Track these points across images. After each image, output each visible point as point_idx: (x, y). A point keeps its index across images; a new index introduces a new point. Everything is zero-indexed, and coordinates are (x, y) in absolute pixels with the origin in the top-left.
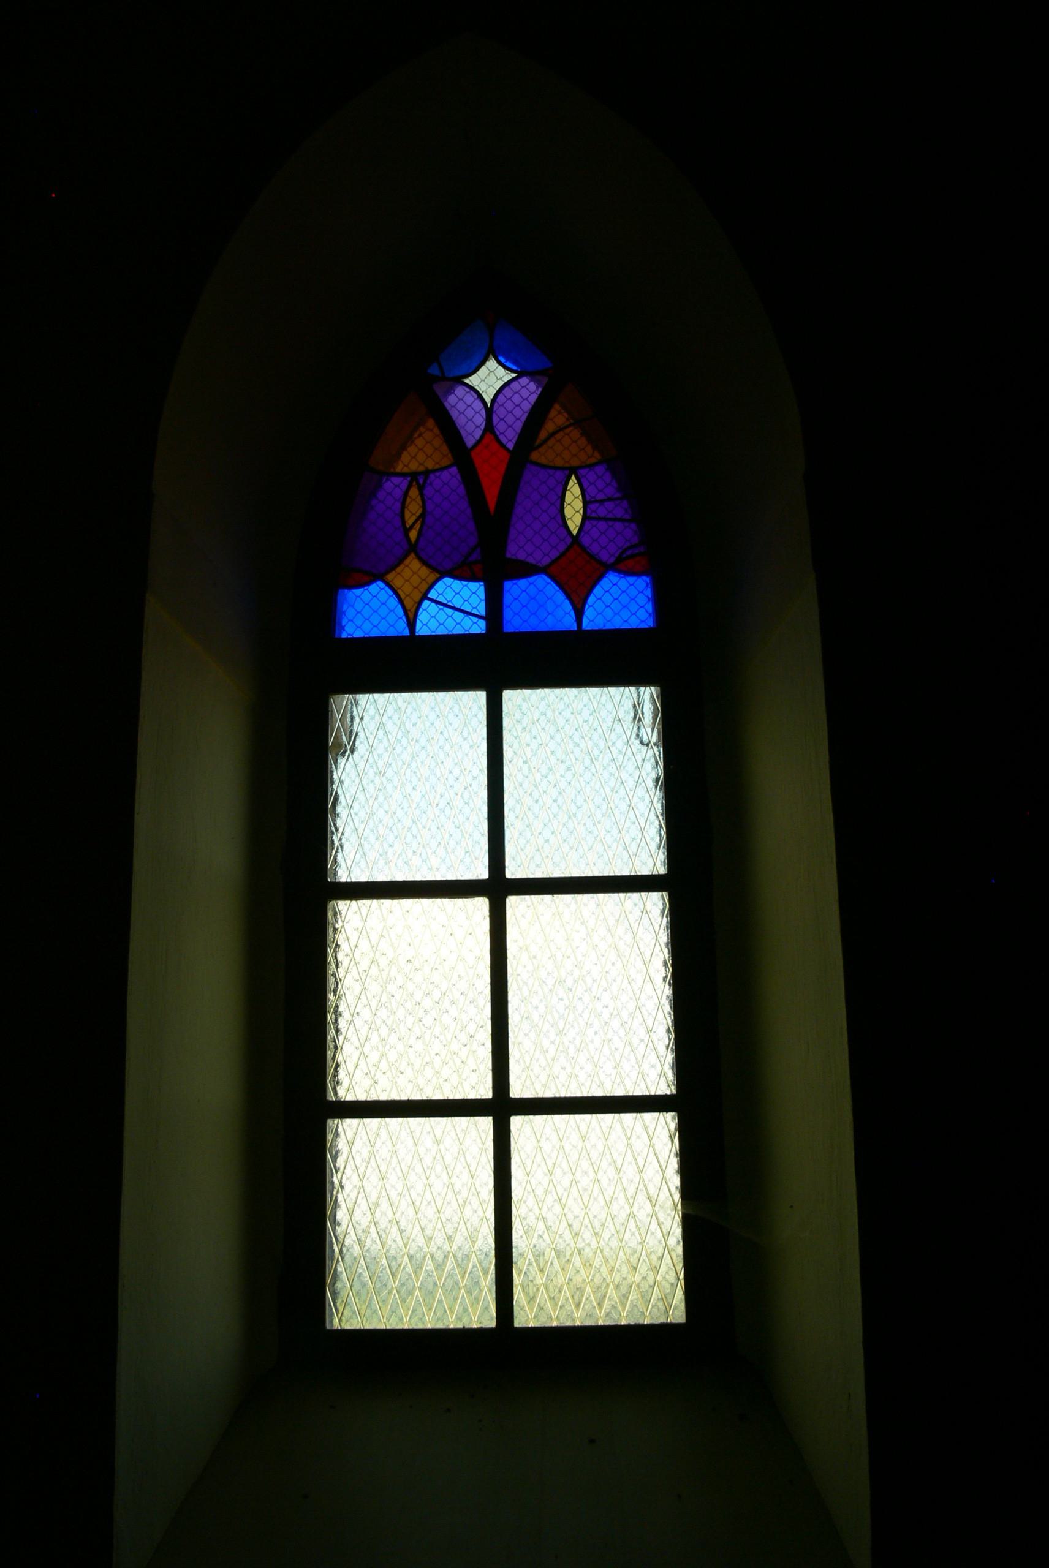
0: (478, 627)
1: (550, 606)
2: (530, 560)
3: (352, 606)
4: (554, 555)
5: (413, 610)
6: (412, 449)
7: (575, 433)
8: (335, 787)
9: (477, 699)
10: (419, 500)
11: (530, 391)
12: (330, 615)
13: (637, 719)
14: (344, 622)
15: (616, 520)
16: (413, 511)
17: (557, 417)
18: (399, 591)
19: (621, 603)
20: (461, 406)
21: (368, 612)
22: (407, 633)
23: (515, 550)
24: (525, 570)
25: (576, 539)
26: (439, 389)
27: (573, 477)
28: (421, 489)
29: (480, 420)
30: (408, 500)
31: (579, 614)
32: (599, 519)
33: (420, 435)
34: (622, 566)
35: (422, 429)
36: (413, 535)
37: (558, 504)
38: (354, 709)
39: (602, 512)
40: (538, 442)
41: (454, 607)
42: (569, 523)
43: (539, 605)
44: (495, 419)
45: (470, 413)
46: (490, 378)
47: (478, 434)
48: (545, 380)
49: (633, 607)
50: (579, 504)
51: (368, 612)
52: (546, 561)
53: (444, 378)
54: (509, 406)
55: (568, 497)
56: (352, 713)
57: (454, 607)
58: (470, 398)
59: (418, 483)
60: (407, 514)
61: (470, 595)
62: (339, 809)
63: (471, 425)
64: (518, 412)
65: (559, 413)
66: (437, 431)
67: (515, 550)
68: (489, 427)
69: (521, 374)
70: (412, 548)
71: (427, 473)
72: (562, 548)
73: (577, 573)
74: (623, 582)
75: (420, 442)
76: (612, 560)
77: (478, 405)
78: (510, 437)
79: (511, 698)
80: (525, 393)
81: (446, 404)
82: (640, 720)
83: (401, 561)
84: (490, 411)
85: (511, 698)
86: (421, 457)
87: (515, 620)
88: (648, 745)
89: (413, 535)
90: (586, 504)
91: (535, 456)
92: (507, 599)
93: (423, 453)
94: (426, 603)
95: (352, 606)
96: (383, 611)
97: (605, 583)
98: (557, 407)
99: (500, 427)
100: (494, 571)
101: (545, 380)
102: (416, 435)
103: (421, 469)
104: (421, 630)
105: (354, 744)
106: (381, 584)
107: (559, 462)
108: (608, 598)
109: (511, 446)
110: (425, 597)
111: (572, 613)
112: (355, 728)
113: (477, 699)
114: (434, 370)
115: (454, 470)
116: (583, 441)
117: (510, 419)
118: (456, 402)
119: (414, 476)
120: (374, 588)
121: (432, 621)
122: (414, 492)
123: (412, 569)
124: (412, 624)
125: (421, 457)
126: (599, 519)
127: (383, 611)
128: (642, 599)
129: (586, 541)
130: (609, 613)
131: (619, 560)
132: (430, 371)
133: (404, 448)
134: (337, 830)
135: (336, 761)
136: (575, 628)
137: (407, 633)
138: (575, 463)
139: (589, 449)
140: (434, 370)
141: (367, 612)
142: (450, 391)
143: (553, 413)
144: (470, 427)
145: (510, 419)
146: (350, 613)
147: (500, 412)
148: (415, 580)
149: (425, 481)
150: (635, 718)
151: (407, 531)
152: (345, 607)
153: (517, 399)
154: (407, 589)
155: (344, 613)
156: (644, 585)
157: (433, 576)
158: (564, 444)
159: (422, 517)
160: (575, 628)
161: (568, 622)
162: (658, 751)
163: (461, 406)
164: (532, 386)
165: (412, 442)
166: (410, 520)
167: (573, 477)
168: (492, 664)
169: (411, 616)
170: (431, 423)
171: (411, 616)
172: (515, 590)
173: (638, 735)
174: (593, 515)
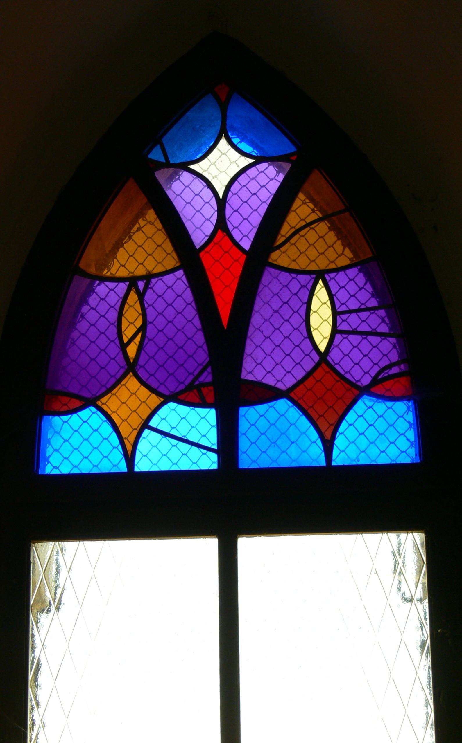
0: (209, 462)
1: (293, 434)
2: (269, 381)
3: (58, 433)
4: (300, 374)
5: (132, 439)
6: (130, 246)
7: (323, 227)
8: (37, 653)
9: (209, 547)
10: (138, 306)
11: (270, 178)
12: (32, 446)
13: (397, 569)
14: (49, 451)
15: (374, 333)
16: (132, 321)
17: (302, 210)
18: (114, 417)
19: (379, 434)
20: (187, 195)
21: (77, 444)
22: (123, 467)
23: (253, 370)
24: (265, 394)
25: (324, 356)
26: (161, 176)
27: (320, 282)
28: (141, 296)
29: (211, 212)
30: (126, 307)
31: (328, 447)
32: (350, 312)
33: (139, 229)
34: (379, 388)
35: (141, 222)
36: (132, 350)
37: (303, 312)
38: (60, 557)
39: (354, 321)
40: (280, 240)
41: (180, 439)
42: (315, 334)
43: (279, 437)
44: (228, 211)
45: (198, 203)
46: (222, 163)
47: (209, 228)
48: (287, 166)
49: (392, 435)
50: (327, 312)
51: (77, 444)
52: (290, 382)
53: (168, 165)
54: (244, 194)
55: (315, 304)
56: (57, 560)
57: (180, 439)
58: (198, 184)
59: (138, 292)
60: (124, 324)
61: (200, 423)
62: (41, 679)
63: (200, 225)
64: (254, 202)
65: (304, 203)
66: (159, 225)
67: (253, 370)
68: (221, 224)
69: (258, 160)
70: (131, 367)
71: (148, 277)
72: (309, 365)
73: (325, 395)
74: (381, 407)
75: (138, 237)
76: (366, 381)
77: (207, 194)
78: (245, 234)
79: (247, 546)
80: (262, 179)
81: (169, 193)
82: (401, 573)
83: (118, 382)
84: (222, 204)
85: (247, 546)
86: (140, 256)
87: (253, 454)
88: (411, 600)
89: (132, 350)
90: (335, 314)
91: (275, 257)
92: (243, 425)
93: (143, 250)
94: (147, 432)
95: (58, 433)
96: (95, 439)
97: (360, 406)
98: (301, 196)
99: (233, 220)
100: (227, 392)
101: (287, 166)
102: (135, 229)
103: (141, 272)
104: (142, 465)
105: (60, 603)
106: (93, 409)
107: (303, 264)
108: (361, 425)
109: (246, 245)
110: (145, 425)
111: (319, 442)
112: (61, 582)
113: (209, 547)
114: (156, 155)
115: (180, 273)
116: (331, 237)
117: (245, 211)
118: (182, 191)
119: (132, 281)
120: (85, 413)
121: (155, 456)
122: (133, 297)
123: (130, 395)
124: (130, 459)
125: (140, 256)
126: (350, 312)
127: (95, 439)
128: (402, 425)
129: (335, 356)
130: (363, 442)
131: (375, 381)
132: (151, 156)
133: (118, 245)
134: (38, 704)
135: (37, 622)
136: (323, 463)
137: (123, 467)
138: (322, 264)
139: (339, 246)
140: (156, 155)
141: (76, 440)
142: (172, 179)
143: (297, 203)
144: (198, 220)
145: (245, 211)
146: (56, 442)
147: (233, 201)
148: (133, 403)
149: (146, 288)
150: (395, 570)
151: (124, 346)
152: (49, 436)
153: (253, 187)
154: (124, 412)
155: (49, 441)
156: (405, 408)
157: (155, 400)
158: (312, 240)
159: (143, 329)
160: (323, 463)
161: (313, 454)
162: (423, 608)
163: (187, 195)
164: (272, 171)
165: (130, 238)
166: (128, 332)
167: (320, 282)
168: (227, 504)
169: (129, 447)
170: (151, 215)
171: (129, 447)
172: (252, 418)
173: (399, 589)
174: (343, 308)
